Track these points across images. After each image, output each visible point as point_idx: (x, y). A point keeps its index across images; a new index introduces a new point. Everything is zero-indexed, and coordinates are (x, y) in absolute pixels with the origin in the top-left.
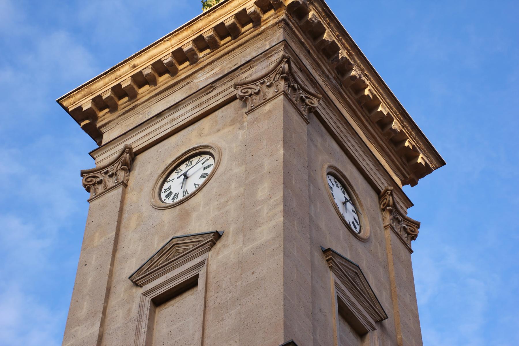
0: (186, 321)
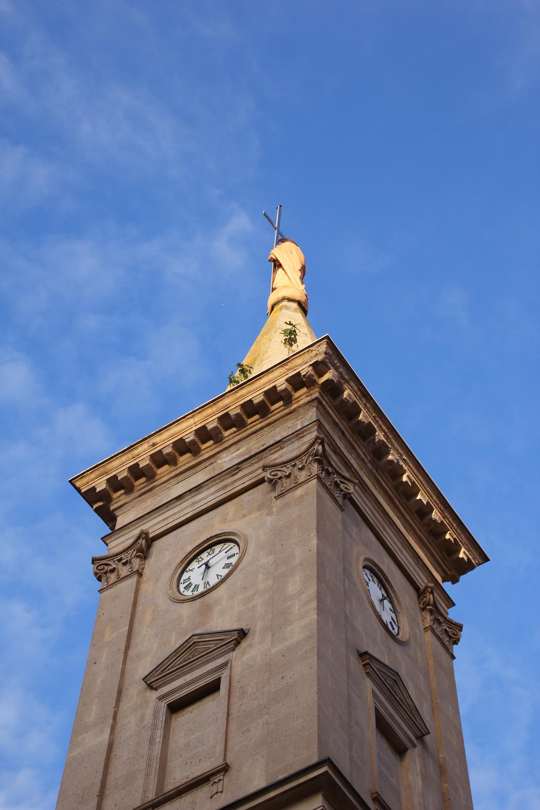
0: (206, 730)
